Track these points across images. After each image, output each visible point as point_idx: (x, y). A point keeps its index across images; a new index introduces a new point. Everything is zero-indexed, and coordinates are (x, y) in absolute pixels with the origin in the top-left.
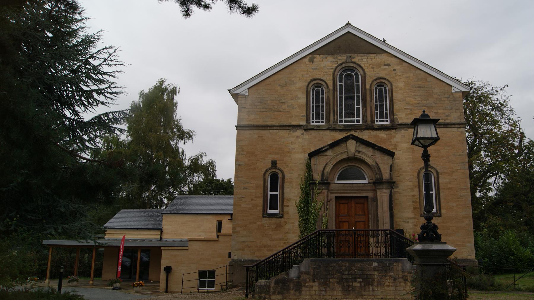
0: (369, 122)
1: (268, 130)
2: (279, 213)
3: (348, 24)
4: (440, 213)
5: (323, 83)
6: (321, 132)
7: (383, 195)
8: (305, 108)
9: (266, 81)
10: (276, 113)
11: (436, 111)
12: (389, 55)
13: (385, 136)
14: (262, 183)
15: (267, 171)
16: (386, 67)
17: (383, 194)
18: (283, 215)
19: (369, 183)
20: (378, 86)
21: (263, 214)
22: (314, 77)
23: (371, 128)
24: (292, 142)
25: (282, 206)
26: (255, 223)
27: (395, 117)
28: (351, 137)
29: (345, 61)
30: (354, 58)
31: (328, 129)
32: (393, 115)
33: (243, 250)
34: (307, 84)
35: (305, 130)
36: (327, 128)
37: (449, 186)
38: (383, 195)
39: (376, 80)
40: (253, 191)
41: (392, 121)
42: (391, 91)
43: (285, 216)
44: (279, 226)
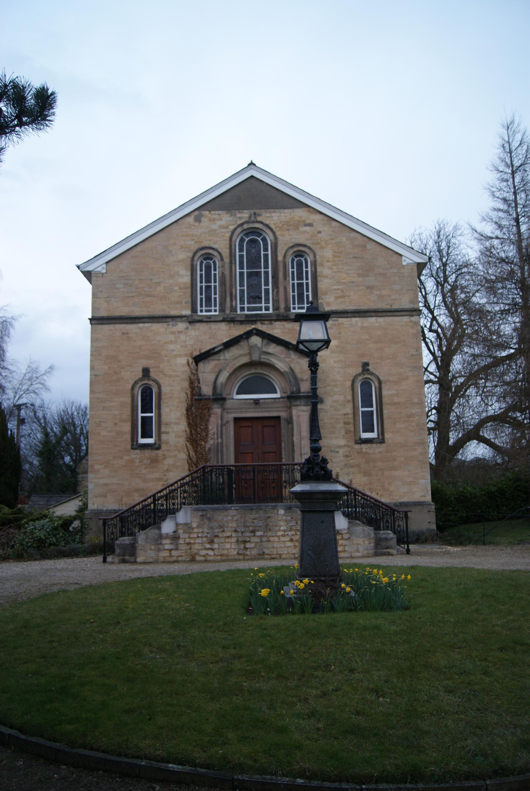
3: (252, 164)
4: (383, 439)
5: (215, 253)
6: (213, 326)
8: (189, 290)
9: (131, 252)
10: (147, 299)
11: (378, 293)
12: (312, 210)
14: (128, 400)
16: (307, 228)
17: (301, 413)
19: (281, 398)
21: (132, 445)
26: (121, 458)
27: (320, 301)
28: (254, 332)
29: (247, 220)
30: (260, 215)
33: (105, 496)
34: (191, 255)
35: (190, 322)
37: (396, 400)
39: (292, 247)
40: (117, 412)
42: (314, 264)
43: (164, 447)
44: (155, 461)
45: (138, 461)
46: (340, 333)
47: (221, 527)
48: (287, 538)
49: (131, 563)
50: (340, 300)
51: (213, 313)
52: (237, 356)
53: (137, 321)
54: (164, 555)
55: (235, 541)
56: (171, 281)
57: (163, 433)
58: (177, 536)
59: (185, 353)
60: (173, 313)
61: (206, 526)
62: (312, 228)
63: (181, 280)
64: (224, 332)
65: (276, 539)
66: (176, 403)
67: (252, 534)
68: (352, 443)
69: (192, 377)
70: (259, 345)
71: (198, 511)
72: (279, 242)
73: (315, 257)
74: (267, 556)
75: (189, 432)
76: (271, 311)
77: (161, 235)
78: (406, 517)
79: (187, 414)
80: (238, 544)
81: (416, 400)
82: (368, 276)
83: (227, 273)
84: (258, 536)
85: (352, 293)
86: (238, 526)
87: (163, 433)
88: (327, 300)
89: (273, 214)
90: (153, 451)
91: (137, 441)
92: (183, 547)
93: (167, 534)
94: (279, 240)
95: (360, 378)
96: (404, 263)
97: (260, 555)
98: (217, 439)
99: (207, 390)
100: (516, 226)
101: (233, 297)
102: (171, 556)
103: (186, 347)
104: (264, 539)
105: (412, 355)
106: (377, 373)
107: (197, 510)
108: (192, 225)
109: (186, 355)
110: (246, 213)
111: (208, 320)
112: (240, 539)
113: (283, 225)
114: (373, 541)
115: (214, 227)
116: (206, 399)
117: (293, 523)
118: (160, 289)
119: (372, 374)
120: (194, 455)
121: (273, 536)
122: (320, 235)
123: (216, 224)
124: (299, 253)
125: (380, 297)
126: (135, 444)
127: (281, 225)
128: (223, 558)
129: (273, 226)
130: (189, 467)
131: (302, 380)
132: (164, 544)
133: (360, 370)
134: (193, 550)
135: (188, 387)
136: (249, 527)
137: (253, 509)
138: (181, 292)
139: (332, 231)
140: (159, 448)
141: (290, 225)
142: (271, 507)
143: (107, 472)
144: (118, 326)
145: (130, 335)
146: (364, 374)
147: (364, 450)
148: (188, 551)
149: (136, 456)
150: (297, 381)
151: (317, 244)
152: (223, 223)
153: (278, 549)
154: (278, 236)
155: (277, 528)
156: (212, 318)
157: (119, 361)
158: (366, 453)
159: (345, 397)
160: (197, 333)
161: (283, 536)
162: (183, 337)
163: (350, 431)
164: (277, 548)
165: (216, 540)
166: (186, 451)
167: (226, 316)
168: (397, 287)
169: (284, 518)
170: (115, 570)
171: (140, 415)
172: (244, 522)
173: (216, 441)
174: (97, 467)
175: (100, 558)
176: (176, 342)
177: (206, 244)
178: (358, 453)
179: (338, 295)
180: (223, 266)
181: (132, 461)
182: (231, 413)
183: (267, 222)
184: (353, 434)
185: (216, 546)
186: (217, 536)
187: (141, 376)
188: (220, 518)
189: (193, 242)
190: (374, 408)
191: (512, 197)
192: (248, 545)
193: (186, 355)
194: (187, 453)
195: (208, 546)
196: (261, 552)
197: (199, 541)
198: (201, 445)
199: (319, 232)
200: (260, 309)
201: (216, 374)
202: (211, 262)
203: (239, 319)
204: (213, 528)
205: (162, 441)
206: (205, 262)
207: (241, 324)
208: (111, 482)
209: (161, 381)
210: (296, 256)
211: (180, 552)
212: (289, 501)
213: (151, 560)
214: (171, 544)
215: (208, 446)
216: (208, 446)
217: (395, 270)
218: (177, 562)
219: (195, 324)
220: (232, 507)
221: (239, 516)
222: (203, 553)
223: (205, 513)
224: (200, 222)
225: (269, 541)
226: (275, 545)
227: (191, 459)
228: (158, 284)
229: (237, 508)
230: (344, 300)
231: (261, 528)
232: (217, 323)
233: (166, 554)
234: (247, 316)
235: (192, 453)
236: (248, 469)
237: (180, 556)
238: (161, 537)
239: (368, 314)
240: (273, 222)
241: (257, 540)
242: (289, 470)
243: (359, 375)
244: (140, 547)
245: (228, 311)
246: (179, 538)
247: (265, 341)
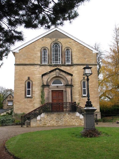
0: (63, 63)
5: (47, 48)
14: (24, 85)
15: (26, 81)
25: (32, 94)
31: (49, 65)
34: (41, 49)
37: (91, 86)
38: (69, 90)
41: (72, 63)
42: (72, 52)
43: (33, 97)
51: (69, 64)
52: (53, 74)
63: (38, 55)
64: (49, 69)
68: (81, 97)
73: (72, 50)
76: (60, 63)
78: (97, 115)
81: (96, 87)
82: (85, 56)
83: (50, 54)
89: (61, 39)
95: (83, 81)
96: (93, 53)
101: (51, 60)
111: (45, 65)
129: (61, 42)
133: (83, 79)
140: (32, 98)
158: (84, 100)
168: (92, 59)
170: (23, 130)
171: (27, 89)
174: (16, 102)
175: (21, 126)
178: (82, 100)
182: (51, 89)
187: (27, 79)
191: (116, 37)
192: (59, 123)
200: (58, 63)
208: (22, 107)
210: (67, 50)
217: (91, 55)
234: (55, 64)
236: (56, 104)
245: (50, 63)
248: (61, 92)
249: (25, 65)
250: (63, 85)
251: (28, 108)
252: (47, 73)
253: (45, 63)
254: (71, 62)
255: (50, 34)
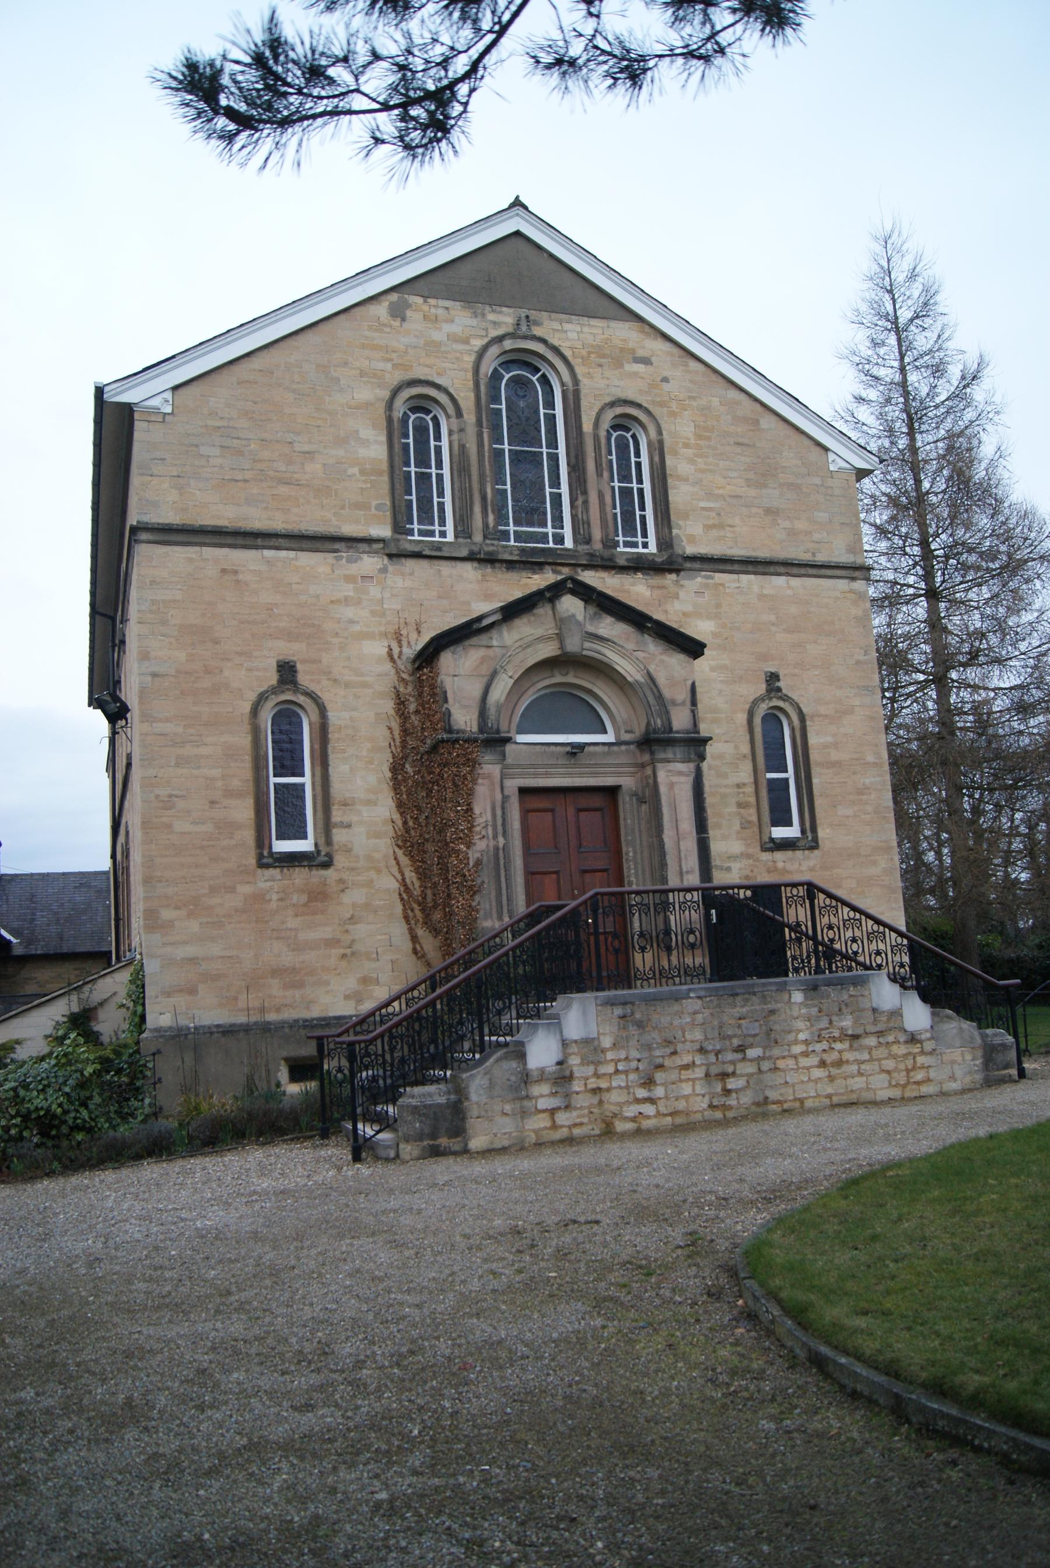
0: (597, 546)
1: (257, 547)
2: (318, 852)
3: (517, 203)
4: (815, 839)
5: (443, 398)
6: (446, 569)
7: (673, 778)
8: (385, 478)
9: (236, 368)
10: (283, 490)
11: (787, 524)
12: (647, 328)
13: (648, 593)
14: (245, 741)
15: (262, 698)
16: (640, 368)
17: (675, 779)
18: (329, 855)
19: (619, 743)
20: (414, 409)
21: (260, 857)
22: (623, 395)
23: (609, 565)
24: (346, 599)
25: (326, 826)
26: (232, 890)
27: (675, 531)
28: (570, 585)
29: (510, 330)
30: (537, 323)
31: (470, 558)
32: (670, 528)
33: (192, 991)
34: (386, 394)
35: (390, 556)
36: (464, 553)
37: (835, 756)
38: (673, 778)
39: (612, 405)
40: (216, 772)
41: (665, 543)
42: (658, 450)
43: (339, 860)
44: (318, 896)
45: (275, 897)
46: (718, 606)
47: (668, 1042)
48: (814, 1060)
49: (455, 1154)
50: (715, 533)
52: (529, 640)
53: (259, 542)
54: (536, 1126)
55: (703, 1075)
56: (341, 453)
57: (336, 825)
58: (567, 1073)
59: (383, 629)
60: (349, 529)
61: (633, 1042)
62: (650, 369)
63: (363, 452)
65: (791, 1063)
66: (365, 753)
67: (739, 1056)
68: (756, 849)
69: (401, 690)
70: (580, 617)
71: (613, 1005)
72: (584, 392)
73: (660, 432)
74: (774, 1107)
75: (399, 823)
77: (309, 335)
79: (394, 778)
80: (709, 1083)
84: (751, 1060)
85: (737, 521)
86: (706, 1039)
87: (336, 825)
88: (690, 531)
89: (567, 326)
90: (314, 872)
91: (270, 847)
92: (583, 1101)
93: (542, 1070)
94: (581, 386)
97: (757, 1104)
98: (495, 837)
99: (464, 718)
100: (908, 434)
102: (554, 1127)
103: (383, 614)
104: (766, 1065)
105: (858, 662)
106: (795, 696)
107: (611, 1003)
108: (385, 325)
109: (385, 635)
110: (509, 315)
112: (714, 1070)
113: (589, 353)
114: (979, 1053)
115: (437, 336)
116: (466, 741)
117: (824, 1024)
118: (314, 468)
119: (786, 698)
120: (415, 880)
121: (784, 1058)
122: (666, 386)
123: (440, 329)
124: (625, 420)
125: (792, 533)
126: (265, 853)
127: (584, 352)
128: (679, 1120)
129: (568, 353)
130: (405, 910)
131: (674, 703)
132: (537, 1098)
133: (762, 688)
134: (606, 1106)
135: (392, 712)
136: (730, 1037)
137: (737, 995)
138: (365, 482)
139: (692, 382)
140: (327, 865)
141: (604, 356)
142: (774, 988)
143: (194, 926)
144: (208, 552)
145: (240, 577)
146: (771, 699)
147: (780, 865)
148: (595, 1110)
149: (269, 884)
150: (663, 704)
151: (662, 404)
152: (455, 328)
153: (797, 1087)
154: (580, 377)
155: (791, 1037)
156: (445, 549)
157: (216, 642)
159: (736, 747)
160: (408, 583)
161: (805, 1054)
162: (374, 591)
163: (749, 822)
164: (793, 1086)
165: (659, 1076)
166: (395, 870)
167: (476, 549)
168: (822, 516)
169: (803, 1011)
172: (721, 1027)
173: (492, 843)
176: (359, 602)
177: (420, 373)
179: (711, 522)
180: (461, 430)
181: (260, 897)
183: (556, 342)
184: (756, 829)
185: (659, 1092)
186: (660, 1067)
188: (665, 1020)
189: (389, 365)
190: (790, 774)
191: (898, 378)
192: (732, 1084)
193: (385, 635)
194: (399, 877)
195: (641, 1093)
196: (761, 1099)
197: (619, 1081)
198: (458, 852)
199: (665, 380)
200: (544, 538)
201: (485, 680)
202: (428, 418)
203: (507, 557)
204: (649, 1047)
205: (336, 847)
206: (413, 417)
207: (508, 569)
209: (325, 697)
211: (575, 1114)
212: (677, 980)
213: (506, 1143)
214: (554, 1094)
215: (473, 855)
216: (473, 855)
217: (817, 481)
218: (570, 1141)
219: (403, 560)
220: (690, 990)
221: (707, 1012)
222: (631, 1111)
223: (628, 1009)
224: (403, 319)
225: (776, 1069)
226: (788, 1079)
227: (407, 889)
228: (309, 455)
229: (702, 993)
230: (722, 533)
231: (758, 1038)
232: (453, 563)
233: (541, 1122)
235: (411, 876)
237: (575, 1125)
238: (526, 1078)
239: (772, 569)
240: (567, 344)
241: (750, 1068)
242: (648, 906)
243: (761, 699)
244: (474, 1112)
245: (478, 538)
246: (571, 1078)
247: (592, 609)
248: (597, 801)
249: (240, 541)
250: (609, 737)
251: (293, 970)
252: (480, 619)
253: (432, 534)
254: (658, 539)
255: (467, 267)
